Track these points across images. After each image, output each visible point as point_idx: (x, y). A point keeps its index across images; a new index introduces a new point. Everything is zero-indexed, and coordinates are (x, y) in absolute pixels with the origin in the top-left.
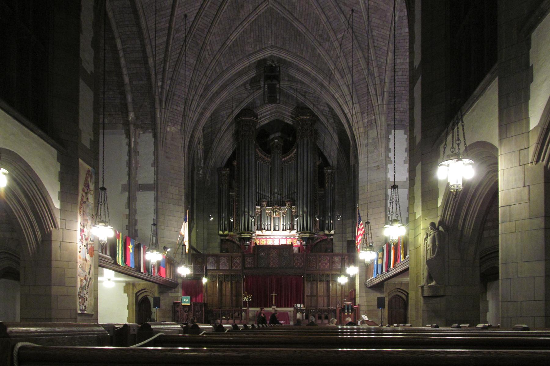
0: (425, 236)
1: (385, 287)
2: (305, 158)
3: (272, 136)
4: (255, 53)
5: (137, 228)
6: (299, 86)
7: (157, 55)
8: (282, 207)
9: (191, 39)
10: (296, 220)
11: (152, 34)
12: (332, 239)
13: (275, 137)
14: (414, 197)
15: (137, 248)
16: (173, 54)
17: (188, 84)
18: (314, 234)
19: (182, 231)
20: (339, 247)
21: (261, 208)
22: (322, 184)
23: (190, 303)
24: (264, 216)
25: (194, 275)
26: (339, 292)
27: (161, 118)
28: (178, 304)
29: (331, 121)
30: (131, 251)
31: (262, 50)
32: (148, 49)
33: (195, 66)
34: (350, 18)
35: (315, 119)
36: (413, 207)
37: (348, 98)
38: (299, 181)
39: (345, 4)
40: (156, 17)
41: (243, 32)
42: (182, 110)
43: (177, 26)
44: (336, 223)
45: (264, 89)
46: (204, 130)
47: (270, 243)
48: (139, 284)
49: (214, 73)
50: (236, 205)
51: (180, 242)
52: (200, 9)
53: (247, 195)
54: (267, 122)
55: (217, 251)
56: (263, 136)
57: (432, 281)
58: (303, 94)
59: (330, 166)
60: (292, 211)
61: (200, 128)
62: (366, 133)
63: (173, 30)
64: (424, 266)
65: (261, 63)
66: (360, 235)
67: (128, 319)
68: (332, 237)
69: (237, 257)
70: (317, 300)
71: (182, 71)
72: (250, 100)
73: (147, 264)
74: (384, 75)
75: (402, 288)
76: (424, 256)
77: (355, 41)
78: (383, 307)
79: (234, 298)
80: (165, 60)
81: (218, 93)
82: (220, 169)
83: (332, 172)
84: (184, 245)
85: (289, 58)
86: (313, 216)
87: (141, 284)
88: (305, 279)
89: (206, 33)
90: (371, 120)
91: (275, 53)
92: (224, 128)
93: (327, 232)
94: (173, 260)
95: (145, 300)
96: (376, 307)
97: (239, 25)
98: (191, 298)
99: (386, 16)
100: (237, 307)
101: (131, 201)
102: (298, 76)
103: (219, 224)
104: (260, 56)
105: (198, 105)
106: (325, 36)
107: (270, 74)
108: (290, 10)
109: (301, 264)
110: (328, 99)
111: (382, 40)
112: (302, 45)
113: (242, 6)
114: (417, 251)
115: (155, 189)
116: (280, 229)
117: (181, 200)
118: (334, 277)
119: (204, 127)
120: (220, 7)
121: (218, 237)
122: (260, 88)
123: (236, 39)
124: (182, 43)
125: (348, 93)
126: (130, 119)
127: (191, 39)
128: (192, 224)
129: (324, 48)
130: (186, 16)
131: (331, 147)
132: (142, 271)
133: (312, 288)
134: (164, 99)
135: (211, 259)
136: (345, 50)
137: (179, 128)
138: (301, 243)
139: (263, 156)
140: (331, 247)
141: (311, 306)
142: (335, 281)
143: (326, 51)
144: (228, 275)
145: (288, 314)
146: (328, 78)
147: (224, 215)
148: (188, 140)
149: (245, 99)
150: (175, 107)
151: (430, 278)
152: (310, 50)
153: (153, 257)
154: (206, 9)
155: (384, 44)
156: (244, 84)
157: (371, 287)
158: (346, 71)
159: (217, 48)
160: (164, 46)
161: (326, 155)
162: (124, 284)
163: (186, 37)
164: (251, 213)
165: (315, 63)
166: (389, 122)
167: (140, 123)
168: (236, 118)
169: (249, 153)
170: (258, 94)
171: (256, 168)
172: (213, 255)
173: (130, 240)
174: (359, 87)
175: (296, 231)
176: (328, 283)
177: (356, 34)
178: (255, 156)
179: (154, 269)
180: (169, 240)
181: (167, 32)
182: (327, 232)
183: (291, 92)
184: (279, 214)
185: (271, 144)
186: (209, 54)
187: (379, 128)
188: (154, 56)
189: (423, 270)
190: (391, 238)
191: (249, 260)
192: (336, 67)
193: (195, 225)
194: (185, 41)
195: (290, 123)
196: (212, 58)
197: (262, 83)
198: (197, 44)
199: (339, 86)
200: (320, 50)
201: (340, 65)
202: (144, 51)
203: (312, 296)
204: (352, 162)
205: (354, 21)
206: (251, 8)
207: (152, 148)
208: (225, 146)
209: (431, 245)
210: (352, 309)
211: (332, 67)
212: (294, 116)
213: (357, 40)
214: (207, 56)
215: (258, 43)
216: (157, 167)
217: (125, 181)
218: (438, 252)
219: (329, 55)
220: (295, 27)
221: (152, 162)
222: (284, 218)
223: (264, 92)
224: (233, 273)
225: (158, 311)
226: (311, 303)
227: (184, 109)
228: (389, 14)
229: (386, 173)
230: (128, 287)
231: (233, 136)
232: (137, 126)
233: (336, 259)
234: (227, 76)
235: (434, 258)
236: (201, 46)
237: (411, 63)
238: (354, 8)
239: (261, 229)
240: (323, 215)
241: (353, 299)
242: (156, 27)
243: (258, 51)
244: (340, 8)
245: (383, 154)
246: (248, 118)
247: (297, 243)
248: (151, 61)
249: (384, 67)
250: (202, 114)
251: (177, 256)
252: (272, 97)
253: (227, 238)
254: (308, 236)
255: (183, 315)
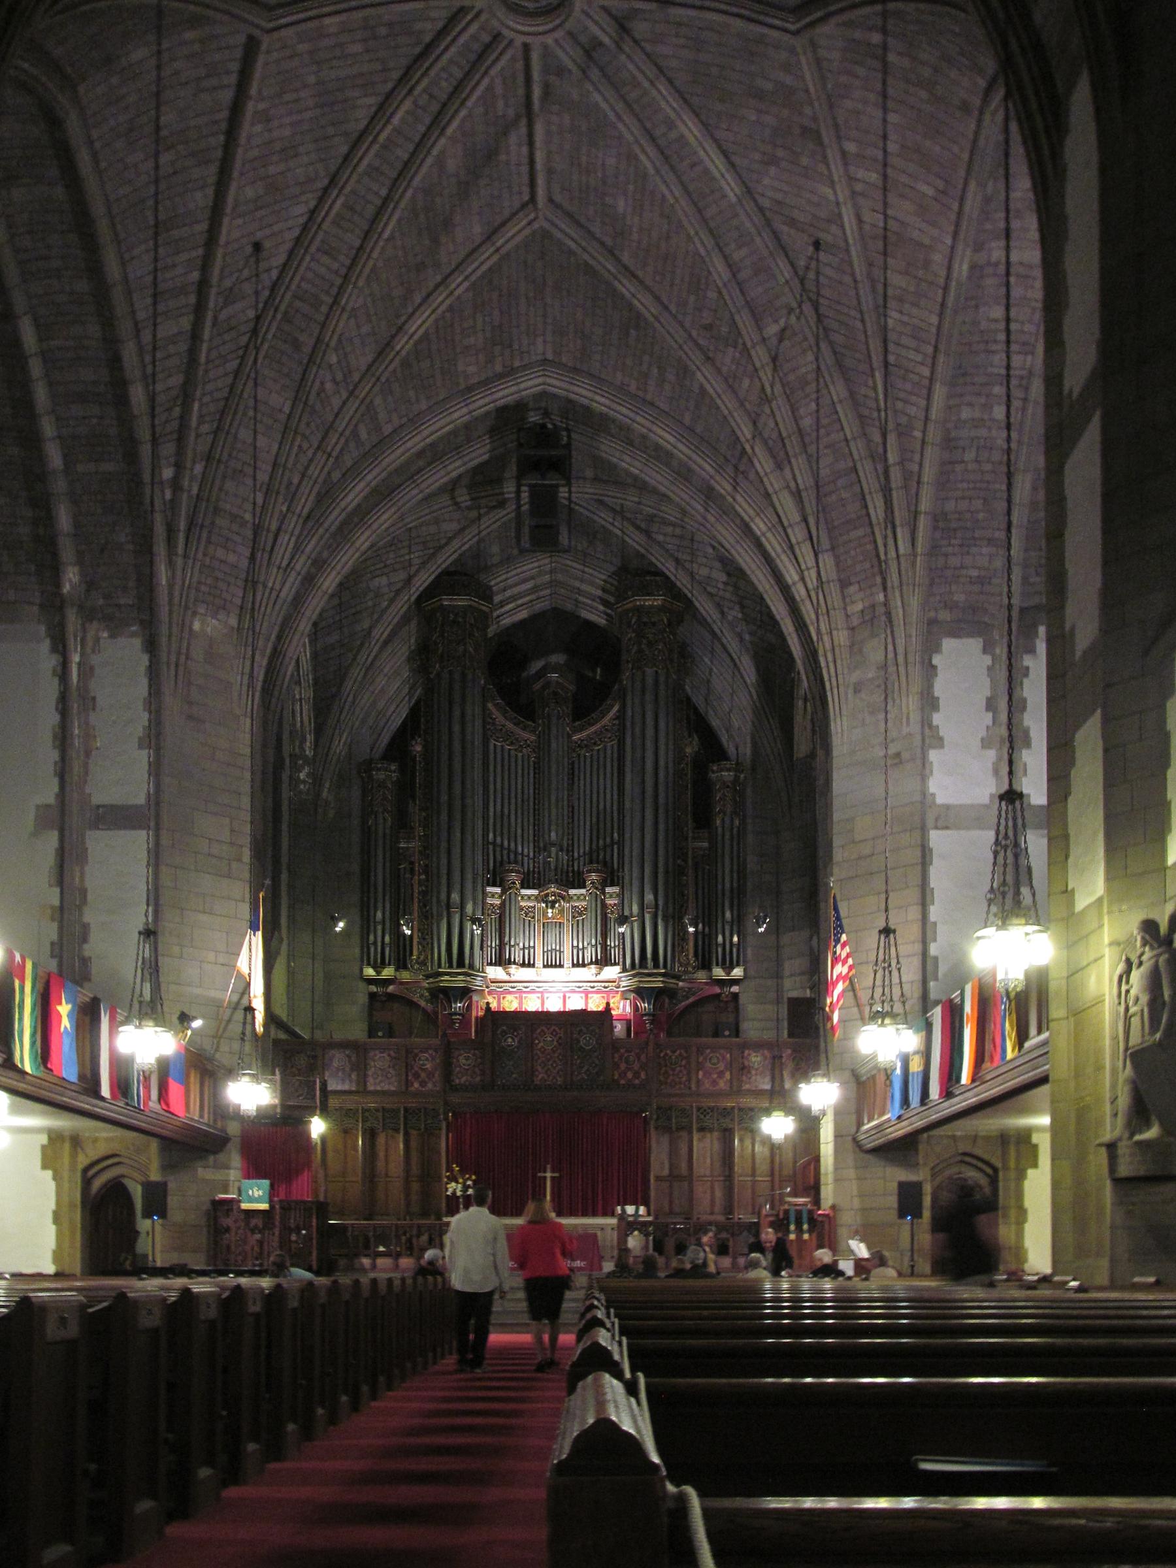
0: (1121, 967)
1: (922, 1147)
2: (650, 732)
3: (536, 666)
4: (486, 383)
5: (88, 950)
6: (630, 499)
7: (160, 376)
8: (572, 892)
9: (275, 325)
10: (621, 930)
11: (143, 304)
12: (735, 996)
13: (551, 669)
14: (1066, 837)
15: (88, 1016)
16: (211, 375)
17: (262, 477)
18: (678, 978)
19: (242, 964)
20: (759, 1018)
21: (504, 892)
22: (703, 820)
23: (271, 1202)
24: (515, 920)
25: (283, 1105)
26: (763, 1167)
27: (171, 586)
28: (228, 1206)
29: (735, 613)
30: (66, 1023)
31: (510, 372)
32: (129, 352)
33: (289, 416)
34: (807, 268)
35: (681, 608)
36: (1065, 869)
37: (797, 534)
38: (628, 805)
39: (792, 222)
40: (156, 246)
41: (450, 309)
42: (244, 563)
43: (228, 283)
44: (751, 940)
45: (519, 507)
46: (314, 637)
47: (532, 1004)
48: (95, 1140)
49: (352, 445)
50: (420, 883)
51: (235, 998)
52: (306, 224)
53: (456, 851)
54: (523, 615)
55: (358, 1032)
56: (507, 659)
57: (1148, 1125)
58: (643, 525)
59: (727, 759)
60: (604, 906)
61: (304, 626)
62: (855, 648)
63: (214, 291)
64: (1114, 1071)
65: (508, 418)
66: (840, 977)
67: (57, 1257)
68: (735, 989)
69: (425, 1050)
70: (691, 1191)
71: (245, 434)
72: (467, 542)
73: (121, 1066)
74: (917, 457)
75: (978, 1152)
76: (1115, 1038)
77: (823, 346)
78: (917, 1214)
79: (415, 1186)
80: (186, 395)
81: (360, 516)
82: (367, 766)
83: (737, 778)
84: (250, 1010)
85: (600, 402)
86: (674, 918)
87: (102, 1139)
88: (652, 1123)
89: (324, 309)
90: (873, 606)
91: (557, 384)
92: (381, 632)
93: (718, 973)
94: (211, 1060)
95: (117, 1192)
96: (894, 1214)
97: (437, 286)
98: (272, 1186)
99: (927, 263)
100: (425, 1214)
101: (67, 863)
102: (630, 464)
103: (365, 946)
104: (505, 394)
105: (297, 549)
106: (725, 329)
107: (538, 451)
108: (609, 242)
109: (637, 1075)
110: (727, 535)
111: (913, 343)
112: (646, 358)
113: (448, 224)
114: (1077, 1024)
115: (152, 824)
116: (567, 963)
117: (239, 860)
118: (748, 1118)
119: (315, 624)
120: (374, 221)
121: (362, 985)
122: (502, 504)
123: (426, 333)
124: (244, 339)
125: (796, 517)
126: (66, 588)
127: (275, 325)
128: (274, 943)
129: (719, 371)
130: (257, 247)
131: (731, 699)
132: (105, 1091)
133: (673, 1153)
134: (182, 525)
135: (338, 1059)
136: (791, 377)
137: (233, 621)
138: (636, 1008)
139: (510, 725)
140: (731, 1018)
141: (671, 1212)
142: (753, 1132)
143: (726, 379)
144: (397, 1111)
145: (595, 1235)
146: (730, 470)
147: (379, 915)
148: (265, 662)
149: (450, 539)
150: (220, 553)
151: (1140, 1112)
152: (671, 377)
153: (144, 1044)
154: (325, 226)
155: (919, 358)
156: (451, 488)
157: (875, 1151)
158: (793, 445)
159: (361, 359)
160: (183, 347)
161: (715, 723)
162: (44, 1139)
163: (258, 318)
164: (469, 908)
165: (687, 420)
166: (932, 614)
167: (101, 602)
168: (419, 600)
169: (463, 715)
170: (494, 521)
171: (486, 765)
172: (344, 1045)
173: (63, 986)
174: (834, 497)
175: (618, 969)
176: (727, 1136)
177: (826, 321)
178: (484, 723)
179: (148, 1088)
180: (198, 991)
181: (192, 299)
182: (718, 973)
183: (603, 518)
184: (561, 911)
185: (537, 686)
186: (334, 380)
187: (900, 632)
188: (150, 379)
189: (1114, 1086)
190: (1000, 976)
191: (464, 1060)
192: (757, 433)
193: (284, 948)
194: (255, 332)
195: (602, 621)
196: (345, 395)
197: (509, 488)
198: (297, 345)
199: (767, 495)
200: (706, 378)
201: (772, 424)
202: (115, 362)
203: (674, 1177)
204: (802, 748)
205: (822, 279)
206: (477, 229)
207: (142, 688)
208: (385, 690)
209: (1145, 999)
210: (812, 1221)
211: (745, 431)
212: (612, 599)
213: (831, 343)
214: (329, 386)
215: (498, 349)
216: (158, 749)
217: (48, 793)
218: (1170, 1025)
219: (735, 392)
220: (623, 297)
221: (140, 732)
222: (578, 927)
223: (519, 515)
224: (412, 1105)
225: (158, 1228)
226: (671, 1203)
227: (252, 558)
228: (937, 258)
229: (924, 778)
230: (54, 1151)
231: (409, 660)
232: (89, 614)
233: (755, 1059)
234: (395, 457)
235: (1160, 1044)
236: (307, 350)
237: (1053, 380)
238: (823, 236)
239: (502, 961)
240: (708, 917)
241: (813, 1189)
242: (155, 278)
243: (500, 376)
244: (776, 235)
245: (915, 717)
246: (461, 602)
247: (622, 1008)
248: (137, 395)
249: (918, 434)
250: (309, 580)
251: (224, 1048)
252: (544, 527)
253: (391, 988)
254: (657, 983)
255: (245, 1242)
